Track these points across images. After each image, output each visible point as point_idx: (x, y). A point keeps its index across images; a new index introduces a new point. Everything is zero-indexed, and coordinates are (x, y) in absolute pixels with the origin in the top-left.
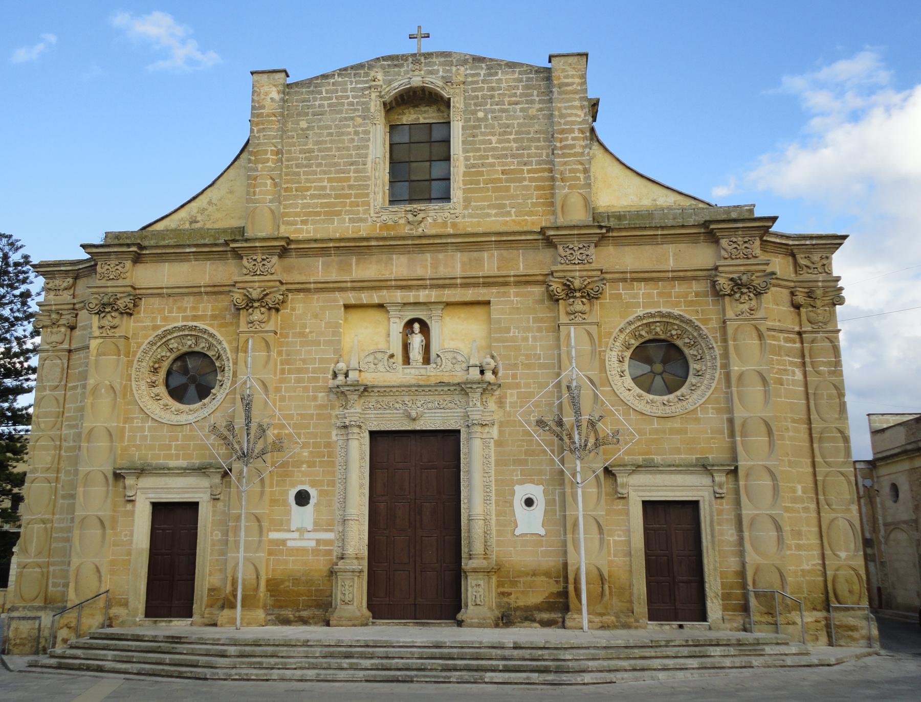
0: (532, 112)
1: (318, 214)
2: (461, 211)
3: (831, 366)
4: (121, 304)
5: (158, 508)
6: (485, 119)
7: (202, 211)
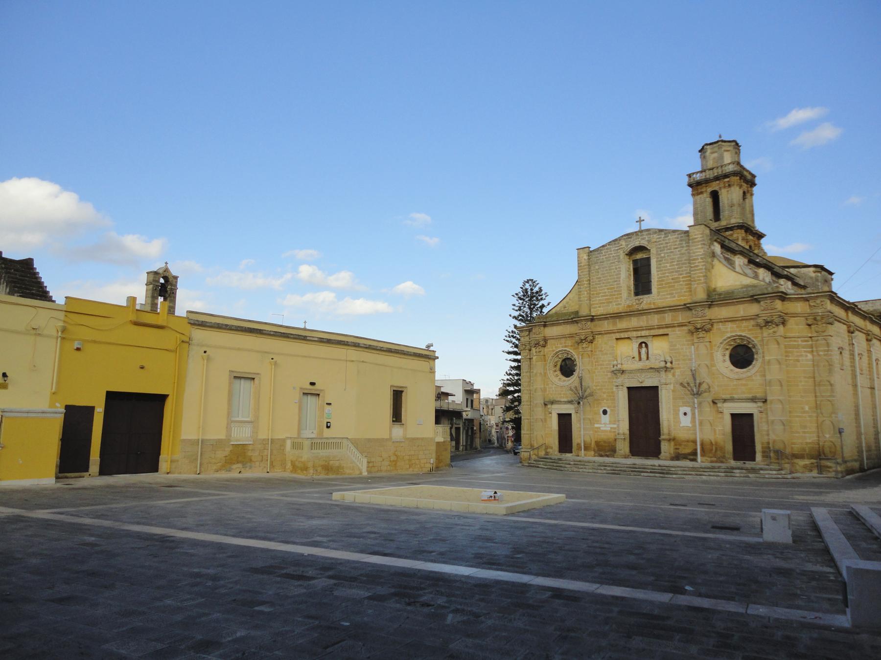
0: (683, 251)
2: (657, 297)
4: (541, 343)
5: (560, 416)
7: (567, 303)
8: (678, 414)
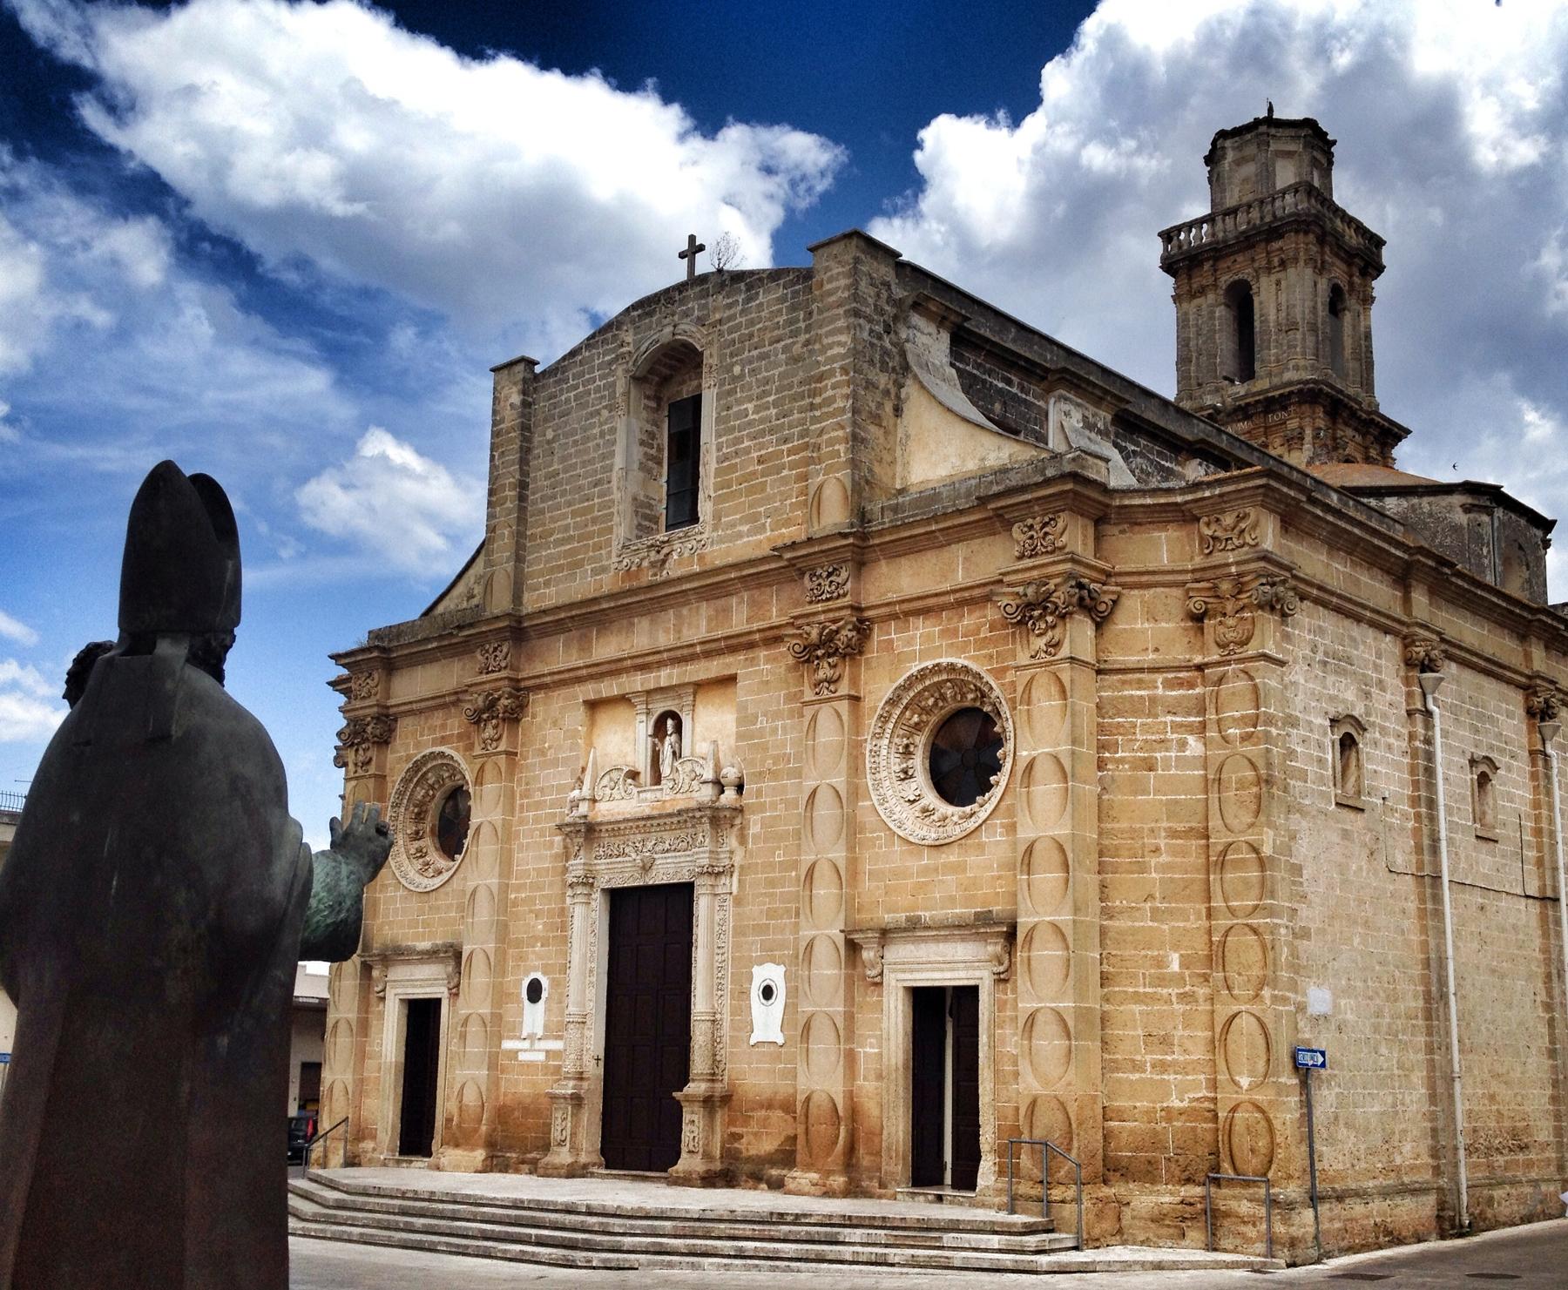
1: (560, 568)
3: (1246, 725)
6: (742, 376)
8: (744, 994)
